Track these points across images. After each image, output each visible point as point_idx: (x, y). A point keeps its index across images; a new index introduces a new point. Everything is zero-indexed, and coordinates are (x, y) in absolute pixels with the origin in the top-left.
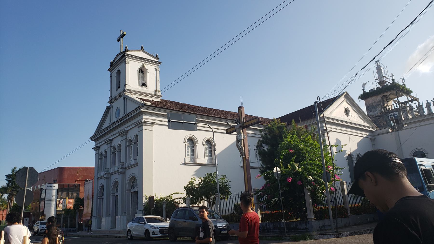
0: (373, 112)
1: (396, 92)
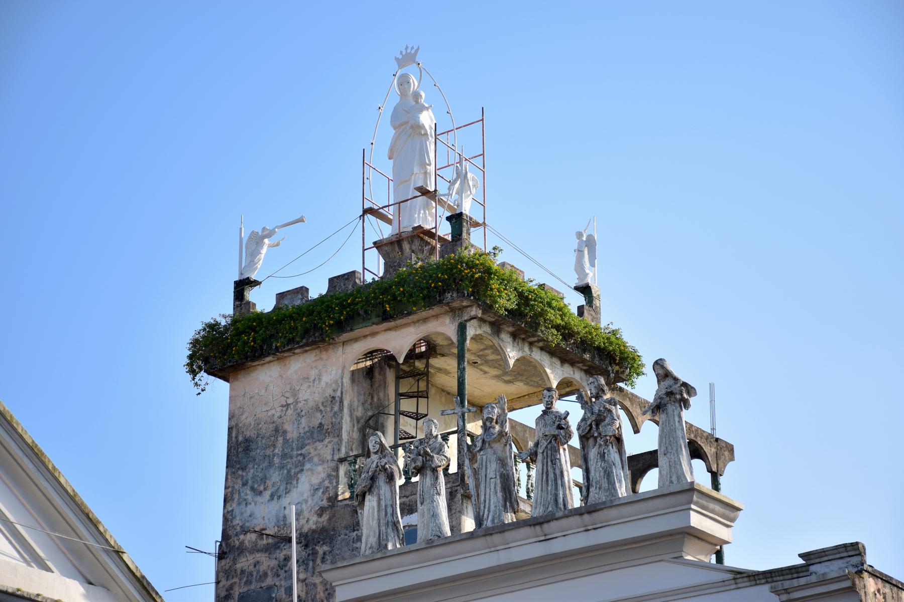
0: (267, 495)
1: (462, 329)
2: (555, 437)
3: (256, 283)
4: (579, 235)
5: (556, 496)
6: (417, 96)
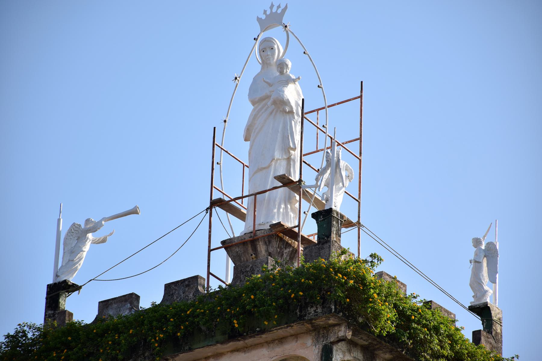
3: (75, 288)
4: (477, 242)
6: (282, 65)
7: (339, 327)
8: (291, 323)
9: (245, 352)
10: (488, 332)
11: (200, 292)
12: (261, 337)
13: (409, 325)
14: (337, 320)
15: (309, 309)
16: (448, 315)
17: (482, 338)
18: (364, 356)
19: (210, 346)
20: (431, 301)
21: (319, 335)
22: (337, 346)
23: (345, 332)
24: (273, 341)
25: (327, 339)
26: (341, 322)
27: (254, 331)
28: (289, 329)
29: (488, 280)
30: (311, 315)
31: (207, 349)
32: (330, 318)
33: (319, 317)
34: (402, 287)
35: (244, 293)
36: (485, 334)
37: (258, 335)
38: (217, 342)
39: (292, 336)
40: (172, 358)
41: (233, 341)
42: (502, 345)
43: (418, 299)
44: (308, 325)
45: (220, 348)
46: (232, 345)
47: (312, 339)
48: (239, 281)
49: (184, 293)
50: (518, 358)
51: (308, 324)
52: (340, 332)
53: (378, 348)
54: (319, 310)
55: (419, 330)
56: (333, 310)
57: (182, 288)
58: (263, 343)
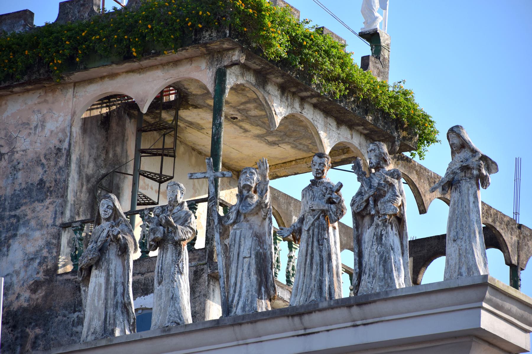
2: (324, 213)
5: (321, 283)
7: (233, 52)
8: (186, 46)
9: (140, 73)
10: (376, 58)
11: (96, 12)
12: (156, 59)
13: (301, 51)
14: (231, 44)
15: (204, 33)
16: (339, 41)
17: (371, 63)
18: (256, 80)
19: (105, 66)
20: (323, 27)
21: (213, 58)
22: (231, 70)
23: (239, 56)
24: (168, 63)
25: (221, 62)
26: (235, 47)
27: (150, 53)
28: (184, 52)
29: (379, 6)
30: (206, 38)
31: (103, 68)
32: (224, 42)
33: (214, 41)
34: (295, 13)
35: (139, 20)
36: (373, 59)
37: (153, 57)
38: (113, 63)
39: (186, 59)
40: (68, 76)
41: (128, 62)
42: (389, 70)
43: (311, 25)
44: (202, 49)
45: (115, 68)
46: (127, 66)
47: (207, 62)
48: (135, 3)
49: (79, 12)
50: (404, 83)
51: (203, 48)
52: (234, 57)
53: (270, 73)
54: (214, 34)
55: (311, 55)
56: (228, 35)
57: (77, 7)
58: (158, 65)
